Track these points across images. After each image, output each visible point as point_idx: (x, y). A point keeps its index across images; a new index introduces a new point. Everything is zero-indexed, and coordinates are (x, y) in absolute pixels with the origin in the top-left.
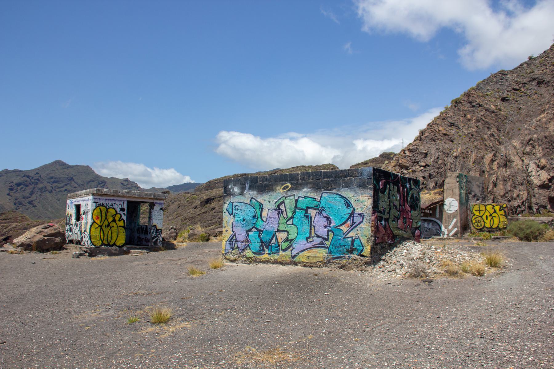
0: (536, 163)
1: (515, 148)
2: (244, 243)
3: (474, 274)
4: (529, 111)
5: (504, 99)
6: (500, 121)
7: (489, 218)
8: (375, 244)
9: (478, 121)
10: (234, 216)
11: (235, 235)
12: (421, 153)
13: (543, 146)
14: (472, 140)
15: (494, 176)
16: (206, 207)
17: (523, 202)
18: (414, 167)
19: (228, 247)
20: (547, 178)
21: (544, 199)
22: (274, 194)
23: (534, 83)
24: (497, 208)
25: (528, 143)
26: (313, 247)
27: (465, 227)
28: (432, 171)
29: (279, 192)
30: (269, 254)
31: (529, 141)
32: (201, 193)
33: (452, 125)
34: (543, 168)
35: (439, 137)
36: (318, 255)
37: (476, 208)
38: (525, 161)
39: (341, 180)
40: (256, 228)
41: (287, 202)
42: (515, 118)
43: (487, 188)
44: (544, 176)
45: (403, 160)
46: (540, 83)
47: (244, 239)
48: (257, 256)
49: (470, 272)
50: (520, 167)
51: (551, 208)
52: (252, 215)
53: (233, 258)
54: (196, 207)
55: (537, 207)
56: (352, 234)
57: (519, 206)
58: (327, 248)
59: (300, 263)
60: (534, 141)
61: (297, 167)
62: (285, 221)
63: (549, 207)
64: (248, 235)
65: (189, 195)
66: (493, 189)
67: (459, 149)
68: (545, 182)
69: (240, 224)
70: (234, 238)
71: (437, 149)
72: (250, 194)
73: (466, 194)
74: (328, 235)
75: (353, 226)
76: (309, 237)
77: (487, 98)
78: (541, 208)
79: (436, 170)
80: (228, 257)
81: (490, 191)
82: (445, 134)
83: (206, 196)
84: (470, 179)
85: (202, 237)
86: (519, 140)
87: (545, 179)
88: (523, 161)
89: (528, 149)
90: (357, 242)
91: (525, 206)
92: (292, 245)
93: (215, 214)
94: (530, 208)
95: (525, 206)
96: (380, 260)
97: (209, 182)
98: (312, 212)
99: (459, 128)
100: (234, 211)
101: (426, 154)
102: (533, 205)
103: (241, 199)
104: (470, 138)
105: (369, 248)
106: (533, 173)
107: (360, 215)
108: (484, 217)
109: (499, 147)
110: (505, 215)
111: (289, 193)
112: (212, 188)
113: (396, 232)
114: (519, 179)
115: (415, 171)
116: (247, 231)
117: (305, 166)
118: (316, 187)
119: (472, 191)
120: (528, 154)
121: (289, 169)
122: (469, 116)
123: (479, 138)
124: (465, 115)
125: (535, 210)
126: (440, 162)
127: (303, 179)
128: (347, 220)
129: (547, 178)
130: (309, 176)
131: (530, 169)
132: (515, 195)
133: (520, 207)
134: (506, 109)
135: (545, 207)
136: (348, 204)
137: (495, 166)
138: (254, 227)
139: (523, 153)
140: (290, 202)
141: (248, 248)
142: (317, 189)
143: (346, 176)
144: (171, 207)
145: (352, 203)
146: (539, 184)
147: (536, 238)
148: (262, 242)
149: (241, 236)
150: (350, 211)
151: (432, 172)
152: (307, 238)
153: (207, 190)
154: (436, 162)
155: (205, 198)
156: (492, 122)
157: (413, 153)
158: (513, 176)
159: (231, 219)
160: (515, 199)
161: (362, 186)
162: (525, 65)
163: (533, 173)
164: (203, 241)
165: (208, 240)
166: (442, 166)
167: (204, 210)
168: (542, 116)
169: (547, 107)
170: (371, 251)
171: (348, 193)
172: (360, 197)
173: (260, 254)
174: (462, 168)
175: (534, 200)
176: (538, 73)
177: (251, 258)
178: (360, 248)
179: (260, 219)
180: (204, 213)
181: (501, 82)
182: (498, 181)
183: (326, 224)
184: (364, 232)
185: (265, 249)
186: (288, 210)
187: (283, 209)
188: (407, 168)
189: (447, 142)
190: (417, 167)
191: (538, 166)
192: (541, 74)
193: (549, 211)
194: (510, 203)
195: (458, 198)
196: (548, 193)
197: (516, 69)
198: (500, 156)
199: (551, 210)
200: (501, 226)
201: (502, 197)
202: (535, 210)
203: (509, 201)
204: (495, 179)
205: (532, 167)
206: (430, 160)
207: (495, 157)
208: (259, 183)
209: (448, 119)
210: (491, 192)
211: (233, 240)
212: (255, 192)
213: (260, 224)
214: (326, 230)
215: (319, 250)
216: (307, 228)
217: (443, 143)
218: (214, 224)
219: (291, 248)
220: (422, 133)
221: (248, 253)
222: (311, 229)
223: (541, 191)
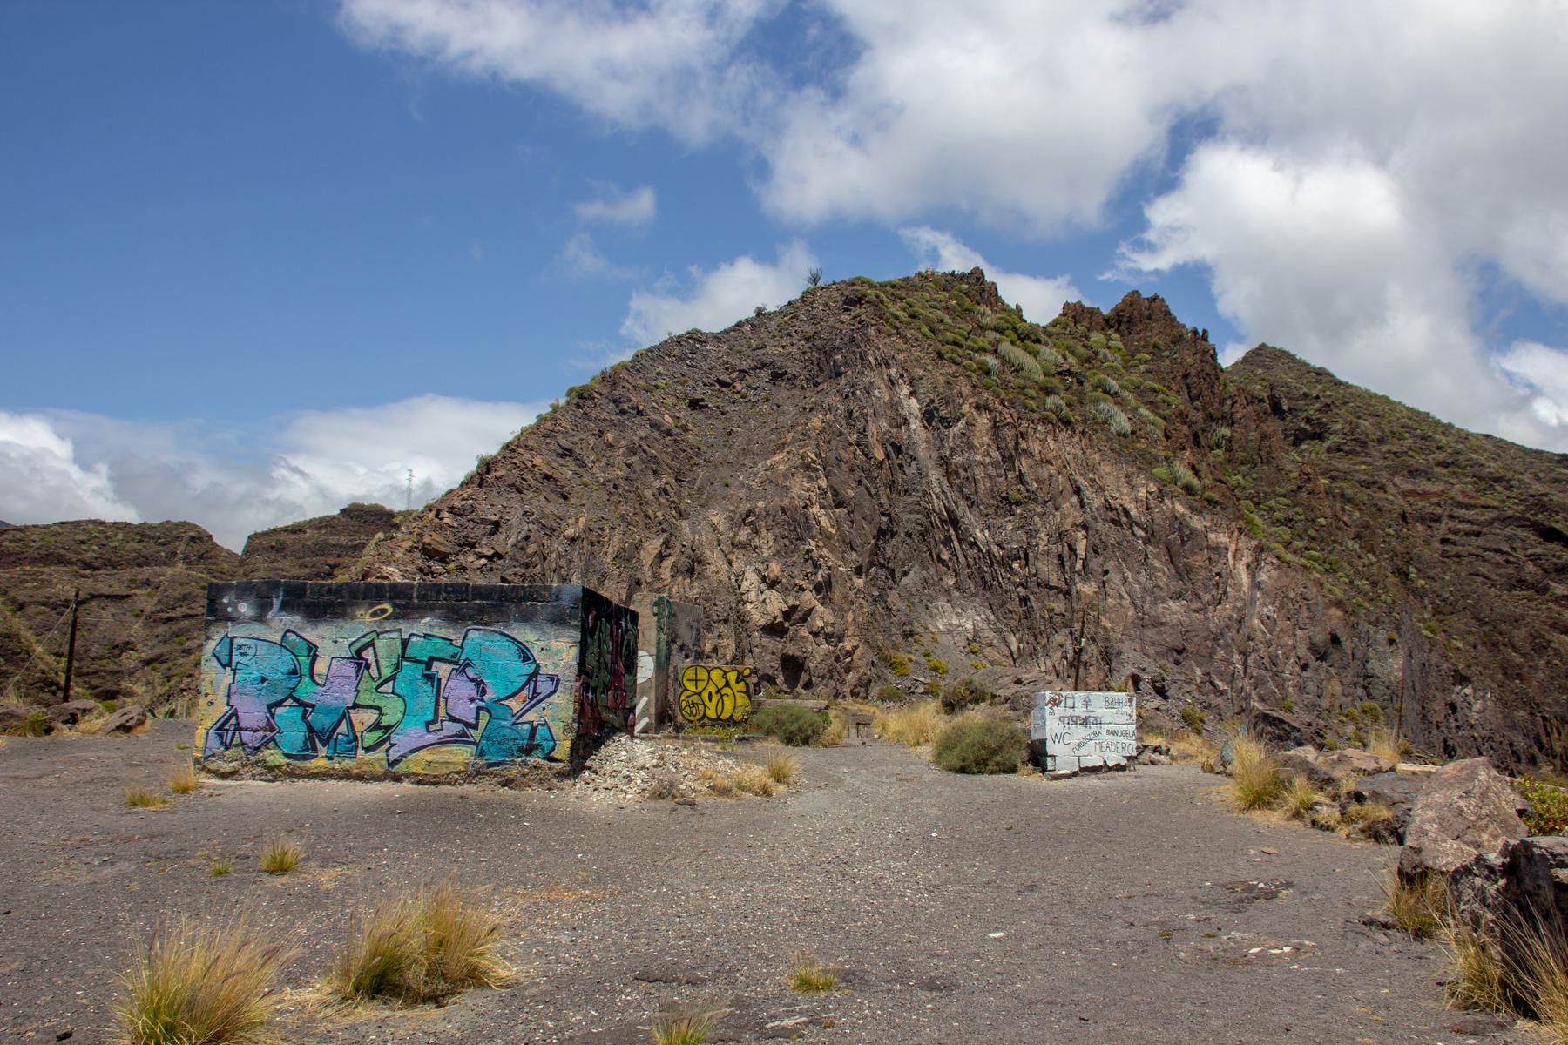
0: (758, 571)
2: (261, 734)
3: (756, 794)
4: (750, 441)
5: (695, 404)
6: (686, 458)
7: (715, 698)
8: (579, 736)
9: (632, 451)
10: (234, 670)
11: (235, 714)
12: (484, 521)
13: (777, 531)
18: (461, 558)
19: (214, 742)
22: (348, 625)
23: (765, 374)
24: (732, 676)
26: (440, 743)
27: (664, 717)
28: (510, 571)
29: (362, 623)
30: (331, 758)
33: (567, 453)
34: (773, 584)
35: (533, 483)
36: (453, 759)
37: (690, 674)
38: (735, 565)
39: (512, 607)
40: (296, 700)
41: (379, 644)
42: (717, 456)
45: (435, 536)
46: (776, 376)
47: (262, 724)
48: (298, 763)
49: (748, 790)
51: (786, 681)
52: (286, 668)
53: (226, 767)
56: (532, 716)
58: (474, 743)
59: (407, 776)
60: (758, 517)
61: (78, 523)
62: (375, 685)
63: (780, 679)
64: (273, 715)
67: (582, 520)
69: (249, 688)
70: (233, 721)
72: (281, 622)
73: (668, 644)
74: (477, 718)
75: (535, 699)
76: (434, 722)
77: (658, 394)
79: (521, 570)
80: (211, 766)
82: (547, 477)
84: (676, 609)
85: (33, 723)
86: (725, 510)
87: (777, 613)
88: (730, 563)
89: (743, 534)
90: (541, 732)
92: (389, 738)
96: (583, 768)
98: (442, 670)
100: (235, 659)
101: (497, 525)
103: (257, 630)
104: (611, 494)
105: (568, 744)
107: (551, 678)
108: (705, 695)
110: (747, 693)
111: (388, 626)
113: (605, 715)
114: (721, 607)
115: (464, 568)
116: (270, 707)
117: (102, 523)
118: (455, 616)
119: (677, 636)
121: (46, 527)
122: (610, 437)
126: (532, 548)
127: (422, 597)
128: (522, 688)
130: (439, 593)
131: (745, 585)
132: (708, 647)
134: (700, 430)
135: (772, 680)
136: (525, 656)
137: (666, 573)
138: (290, 696)
140: (389, 645)
141: (272, 744)
142: (456, 621)
143: (524, 599)
145: (535, 653)
146: (762, 622)
147: (806, 741)
148: (310, 729)
149: (252, 714)
150: (530, 669)
152: (428, 724)
154: (522, 549)
156: (665, 457)
157: (463, 520)
159: (227, 677)
161: (559, 620)
162: (748, 328)
164: (36, 733)
165: (49, 730)
166: (536, 559)
168: (778, 457)
169: (789, 437)
170: (572, 749)
171: (526, 634)
172: (553, 643)
173: (305, 758)
176: (773, 350)
177: (279, 767)
178: (547, 745)
179: (307, 679)
181: (692, 359)
183: (474, 693)
184: (558, 713)
185: (319, 746)
186: (383, 663)
187: (371, 659)
188: (443, 558)
189: (552, 497)
190: (471, 558)
191: (764, 579)
192: (781, 355)
193: (781, 691)
195: (654, 651)
197: (726, 332)
199: (785, 687)
200: (738, 716)
205: (751, 580)
206: (505, 542)
208: (309, 597)
209: (559, 436)
211: (227, 728)
212: (298, 618)
213: (306, 691)
214: (473, 706)
215: (455, 748)
216: (428, 701)
219: (387, 745)
220: (487, 466)
221: (273, 756)
222: (437, 704)
223: (766, 640)
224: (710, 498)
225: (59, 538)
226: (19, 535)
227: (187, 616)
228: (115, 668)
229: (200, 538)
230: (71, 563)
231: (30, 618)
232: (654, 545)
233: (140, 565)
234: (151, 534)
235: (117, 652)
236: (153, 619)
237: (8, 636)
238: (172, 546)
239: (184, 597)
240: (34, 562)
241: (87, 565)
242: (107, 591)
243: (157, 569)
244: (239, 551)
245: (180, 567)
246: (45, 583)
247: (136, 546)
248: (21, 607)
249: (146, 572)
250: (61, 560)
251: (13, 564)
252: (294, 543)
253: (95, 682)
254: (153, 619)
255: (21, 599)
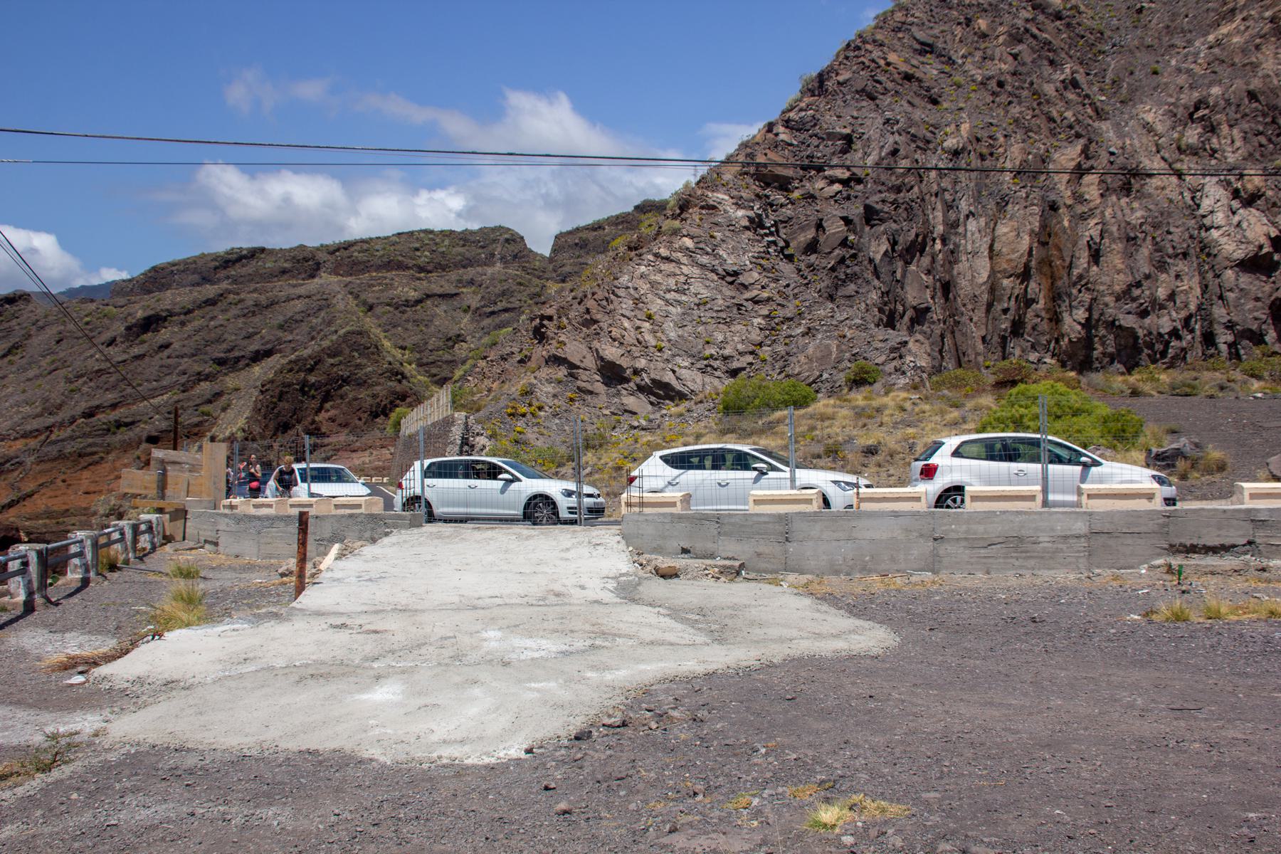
1: (1148, 127)
4: (1174, 16)
9: (1016, 38)
12: (831, 136)
13: (1246, 126)
14: (1003, 98)
15: (1092, 222)
16: (143, 342)
17: (1191, 316)
20: (1268, 236)
21: (1255, 309)
25: (1191, 115)
28: (877, 198)
31: (1197, 108)
32: (130, 302)
33: (926, 49)
34: (1250, 200)
35: (890, 85)
43: (1070, 267)
44: (1257, 228)
45: (772, 155)
50: (1175, 196)
54: (111, 342)
55: (1230, 338)
57: (1175, 334)
60: (1213, 109)
61: (411, 233)
63: (1271, 336)
65: (93, 306)
66: (1087, 270)
67: (965, 128)
68: (1261, 247)
71: (887, 121)
78: (1245, 342)
81: (1080, 277)
82: (908, 77)
83: (144, 308)
86: (1159, 104)
87: (1263, 240)
89: (1192, 135)
91: (1192, 331)
93: (169, 361)
94: (1209, 339)
95: (1192, 331)
97: (154, 269)
99: (951, 62)
101: (848, 139)
102: (1219, 329)
106: (1219, 218)
109: (1096, 124)
112: (163, 287)
115: (813, 197)
117: (431, 232)
120: (1194, 151)
121: (386, 238)
123: (1025, 93)
124: (968, 22)
125: (1223, 348)
129: (1268, 236)
131: (1206, 204)
132: (1162, 293)
133: (1179, 338)
139: (1179, 148)
144: (35, 341)
146: (1239, 255)
151: (874, 200)
153: (149, 292)
155: (140, 314)
158: (1156, 226)
160: (1162, 307)
163: (1219, 218)
167: (136, 351)
168: (1224, 30)
174: (979, 192)
175: (1219, 312)
180: (138, 357)
182: (1106, 241)
188: (784, 185)
189: (917, 101)
190: (820, 184)
191: (1236, 194)
194: (1147, 321)
196: (1267, 288)
198: (1104, 157)
201: (1118, 299)
202: (1223, 348)
203: (1143, 314)
204: (1095, 232)
205: (1214, 196)
206: (866, 158)
207: (1087, 158)
209: (914, 29)
210: (1083, 282)
217: (904, 103)
218: (166, 389)
223: (1245, 279)
224: (1133, 91)
225: (397, 247)
226: (365, 246)
227: (506, 310)
228: (450, 358)
229: (514, 240)
230: (408, 268)
231: (378, 318)
232: (1068, 155)
233: (464, 267)
234: (472, 239)
235: (450, 343)
236: (478, 313)
237: (360, 333)
238: (490, 248)
239: (503, 293)
240: (379, 268)
241: (421, 269)
242: (439, 291)
243: (479, 269)
244: (547, 253)
245: (499, 266)
246: (390, 286)
247: (460, 250)
248: (371, 308)
249: (471, 272)
250: (401, 266)
251: (362, 271)
252: (595, 239)
253: (434, 371)
254: (478, 313)
255: (370, 301)
